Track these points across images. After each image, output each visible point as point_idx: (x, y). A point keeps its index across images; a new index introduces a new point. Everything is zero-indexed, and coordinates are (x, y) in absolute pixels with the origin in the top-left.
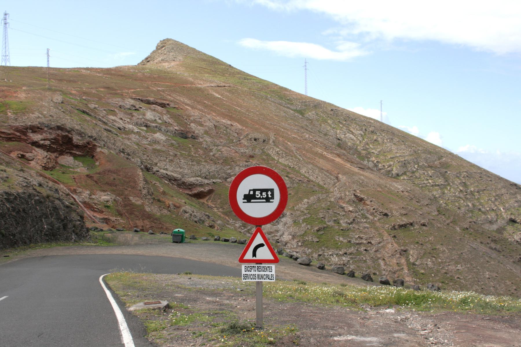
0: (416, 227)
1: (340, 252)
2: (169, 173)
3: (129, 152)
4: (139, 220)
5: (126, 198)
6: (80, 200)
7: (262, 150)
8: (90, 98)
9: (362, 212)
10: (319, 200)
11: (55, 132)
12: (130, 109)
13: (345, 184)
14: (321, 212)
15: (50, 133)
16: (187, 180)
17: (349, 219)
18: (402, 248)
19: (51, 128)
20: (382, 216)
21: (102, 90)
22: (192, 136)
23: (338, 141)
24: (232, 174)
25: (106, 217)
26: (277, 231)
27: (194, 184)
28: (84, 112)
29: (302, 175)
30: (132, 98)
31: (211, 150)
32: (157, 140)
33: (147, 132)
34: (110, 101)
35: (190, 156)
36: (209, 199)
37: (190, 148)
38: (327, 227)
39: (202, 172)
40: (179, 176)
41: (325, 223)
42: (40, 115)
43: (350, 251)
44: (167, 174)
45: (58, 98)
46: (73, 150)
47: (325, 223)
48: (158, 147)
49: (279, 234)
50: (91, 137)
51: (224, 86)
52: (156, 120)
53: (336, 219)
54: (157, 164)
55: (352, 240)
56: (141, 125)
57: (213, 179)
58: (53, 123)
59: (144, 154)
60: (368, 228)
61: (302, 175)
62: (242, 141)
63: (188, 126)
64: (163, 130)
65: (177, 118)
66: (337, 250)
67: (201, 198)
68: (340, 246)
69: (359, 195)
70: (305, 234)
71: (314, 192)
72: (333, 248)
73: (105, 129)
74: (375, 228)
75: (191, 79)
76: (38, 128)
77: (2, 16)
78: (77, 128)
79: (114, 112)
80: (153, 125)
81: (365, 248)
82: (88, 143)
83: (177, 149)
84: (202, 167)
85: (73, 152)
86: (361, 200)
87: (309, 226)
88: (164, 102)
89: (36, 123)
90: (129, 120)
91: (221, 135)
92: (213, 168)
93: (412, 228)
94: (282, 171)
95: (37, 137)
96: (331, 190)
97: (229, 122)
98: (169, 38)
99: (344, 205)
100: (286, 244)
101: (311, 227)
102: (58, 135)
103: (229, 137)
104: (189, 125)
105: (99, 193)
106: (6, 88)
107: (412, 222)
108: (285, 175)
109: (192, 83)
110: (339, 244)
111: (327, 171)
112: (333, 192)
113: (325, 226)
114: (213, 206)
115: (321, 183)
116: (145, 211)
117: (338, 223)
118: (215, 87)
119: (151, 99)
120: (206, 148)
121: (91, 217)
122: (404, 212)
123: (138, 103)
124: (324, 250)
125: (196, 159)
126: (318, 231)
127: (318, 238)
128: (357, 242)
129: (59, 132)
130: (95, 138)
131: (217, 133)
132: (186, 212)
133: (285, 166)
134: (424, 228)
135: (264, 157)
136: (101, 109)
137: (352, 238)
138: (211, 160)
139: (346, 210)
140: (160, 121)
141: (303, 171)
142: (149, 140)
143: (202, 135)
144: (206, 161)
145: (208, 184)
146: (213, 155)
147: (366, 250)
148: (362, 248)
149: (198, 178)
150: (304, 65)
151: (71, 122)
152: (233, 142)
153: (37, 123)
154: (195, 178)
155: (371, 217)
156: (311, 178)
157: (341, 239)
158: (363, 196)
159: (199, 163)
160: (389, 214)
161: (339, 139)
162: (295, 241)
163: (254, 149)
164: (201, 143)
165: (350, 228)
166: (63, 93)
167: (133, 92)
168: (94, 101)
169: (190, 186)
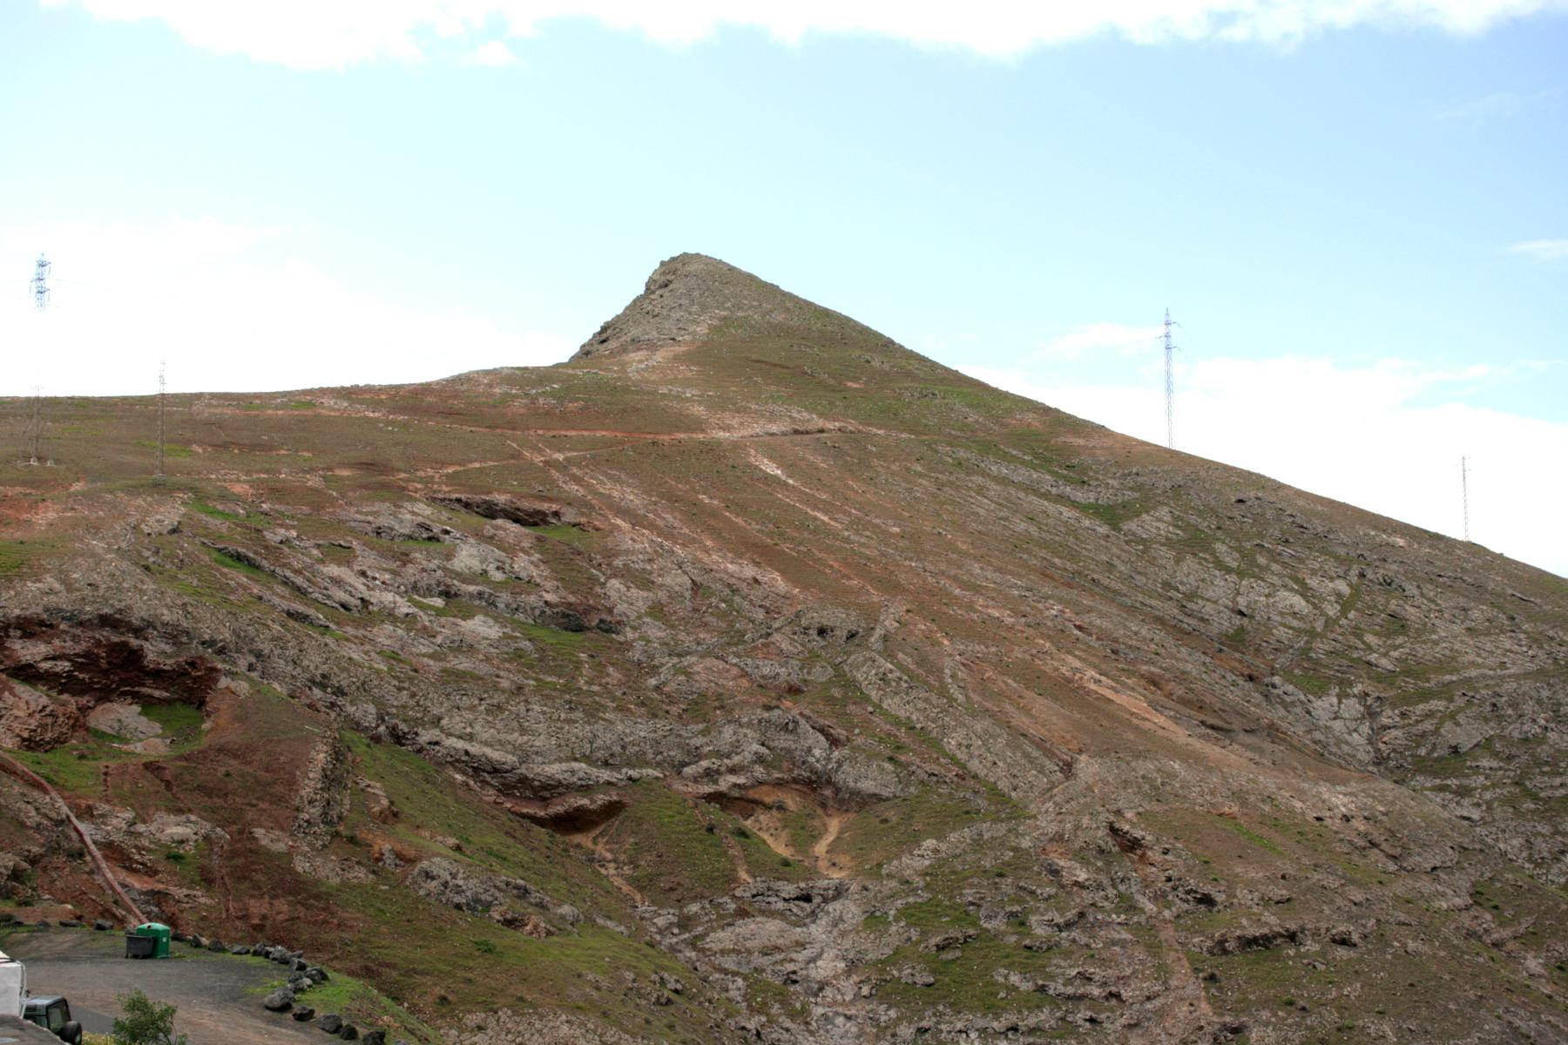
0: (1311, 946)
1: (995, 1024)
2: (475, 749)
3: (344, 683)
4: (262, 897)
5: (245, 833)
6: (98, 837)
7: (836, 667)
8: (282, 508)
9: (1122, 888)
10: (978, 844)
11: (90, 634)
12: (410, 537)
13: (1090, 788)
14: (972, 886)
15: (75, 638)
16: (539, 770)
17: (1062, 912)
18: (1228, 1019)
19: (81, 624)
20: (1191, 906)
21: (345, 473)
22: (602, 621)
23: (1237, 620)
24: (706, 749)
25: (160, 887)
26: (802, 945)
27: (560, 784)
28: (239, 558)
29: (946, 755)
30: (432, 500)
31: (654, 670)
32: (469, 639)
33: (439, 613)
34: (343, 514)
35: (567, 689)
36: (602, 835)
37: (578, 664)
38: (977, 938)
39: (599, 743)
40: (511, 759)
41: (974, 924)
42: (57, 586)
43: (1032, 1021)
44: (467, 753)
45: (170, 513)
46: (144, 685)
47: (974, 924)
48: (462, 664)
49: (807, 953)
50: (211, 643)
51: (822, 431)
52: (485, 572)
53: (1016, 908)
54: (440, 719)
55: (1052, 985)
56: (429, 592)
57: (633, 767)
58: (88, 608)
59: (400, 689)
60: (1123, 944)
61: (946, 755)
62: (776, 637)
63: (598, 589)
64: (502, 606)
65: (562, 561)
66: (984, 1016)
67: (578, 829)
68: (1002, 1004)
69: (1126, 827)
70: (896, 957)
71: (967, 815)
72: (971, 1009)
73: (289, 614)
74: (1149, 946)
75: (699, 410)
76: (42, 623)
77: (33, 271)
78: (167, 617)
79: (344, 552)
80: (472, 588)
81: (1089, 1014)
82: (193, 664)
83: (531, 667)
84: (599, 727)
85: (144, 690)
86: (1131, 845)
87: (914, 934)
88: (545, 506)
89: (35, 610)
90: (387, 576)
91: (708, 618)
92: (640, 730)
93: (1291, 952)
94: (881, 741)
95: (30, 651)
96: (1033, 809)
97: (749, 571)
98: (692, 251)
99: (1062, 863)
100: (821, 989)
101: (923, 933)
102: (98, 643)
103: (731, 624)
104: (603, 585)
105: (163, 817)
106: (19, 489)
107: (1293, 927)
108: (888, 753)
109: (697, 425)
110: (1002, 995)
111: (1040, 744)
112: (1035, 817)
113: (971, 931)
114: (609, 856)
115: (1003, 785)
116: (292, 871)
117: (1022, 924)
118: (784, 434)
119: (501, 498)
120: (639, 663)
121: (112, 888)
122: (1281, 892)
123: (445, 515)
124: (942, 1014)
125: (589, 701)
126: (940, 948)
127: (933, 972)
128: (1070, 990)
129: (106, 635)
130: (224, 648)
131: (695, 610)
132: (429, 876)
133: (897, 722)
134: (1342, 953)
135: (836, 692)
136: (308, 544)
137: (1052, 977)
138: (643, 704)
139: (1067, 878)
140: (498, 576)
141: (951, 743)
142: (439, 640)
143: (639, 617)
144: (620, 709)
145: (609, 783)
146: (657, 688)
147: (1092, 1020)
148: (1083, 1014)
149: (575, 765)
150: (1162, 330)
151: (145, 600)
152: (741, 641)
153: (39, 610)
154: (564, 766)
155: (1150, 907)
156: (974, 765)
157: (1015, 979)
158: (1138, 833)
159: (593, 713)
160: (1220, 898)
161: (1241, 613)
162: (855, 978)
163: (810, 660)
164: (628, 645)
165: (1058, 944)
166: (200, 496)
167: (450, 478)
168: (293, 517)
169: (546, 791)
